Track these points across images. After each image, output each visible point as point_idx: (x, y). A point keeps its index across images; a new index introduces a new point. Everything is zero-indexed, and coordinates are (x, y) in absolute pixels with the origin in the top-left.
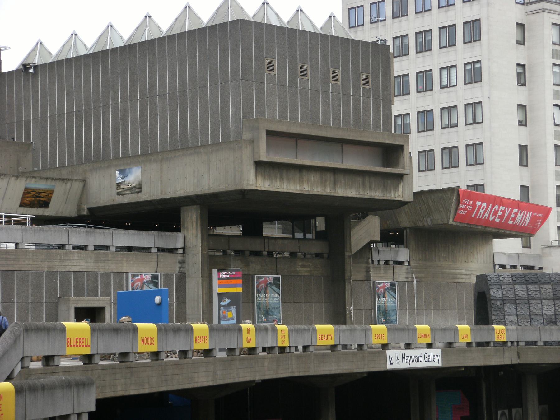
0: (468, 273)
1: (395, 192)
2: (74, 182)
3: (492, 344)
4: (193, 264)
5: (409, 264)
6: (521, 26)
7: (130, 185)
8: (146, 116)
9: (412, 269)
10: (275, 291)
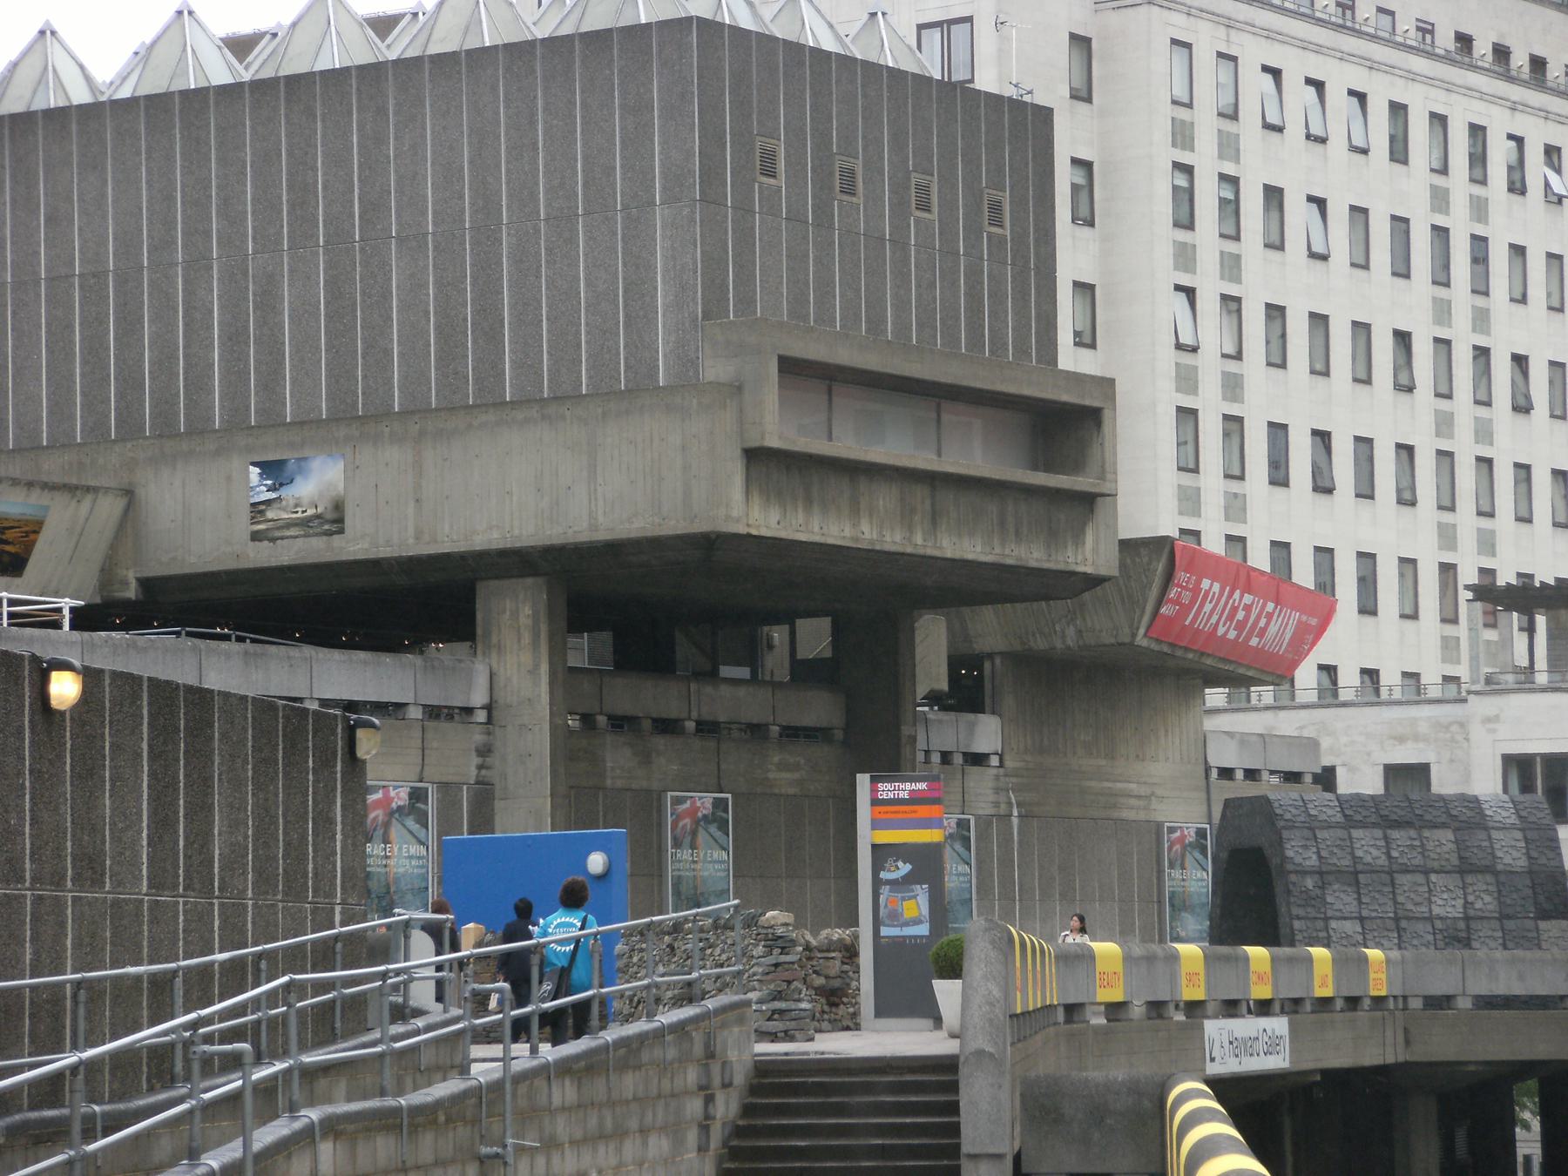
0: (1144, 791)
1: (1077, 548)
2: (100, 495)
3: (1367, 1003)
4: (521, 756)
5: (1001, 765)
6: (1081, 43)
7: (299, 509)
8: (350, 298)
9: (1007, 779)
10: (716, 841)
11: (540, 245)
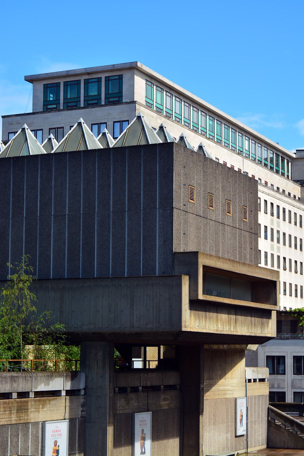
11: (110, 221)
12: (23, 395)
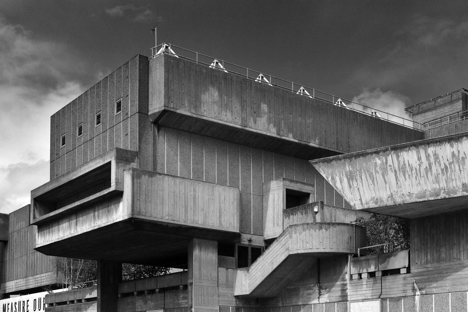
12: (80, 301)
